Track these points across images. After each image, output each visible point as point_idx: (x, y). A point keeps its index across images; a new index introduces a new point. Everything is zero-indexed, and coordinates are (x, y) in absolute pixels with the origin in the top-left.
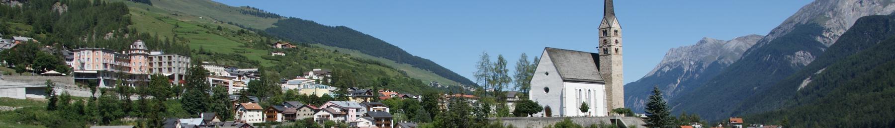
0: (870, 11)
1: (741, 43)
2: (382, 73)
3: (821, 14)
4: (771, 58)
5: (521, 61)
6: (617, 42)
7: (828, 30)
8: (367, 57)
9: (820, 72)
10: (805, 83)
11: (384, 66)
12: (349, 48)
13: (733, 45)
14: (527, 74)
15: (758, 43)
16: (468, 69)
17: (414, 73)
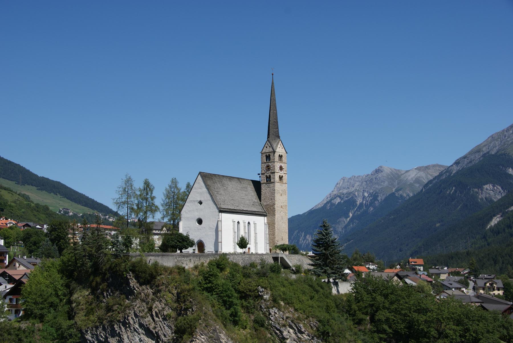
1: (422, 174)
4: (455, 191)
5: (170, 187)
6: (281, 168)
10: (495, 221)
13: (412, 176)
14: (177, 202)
15: (441, 174)
16: (107, 195)
17: (38, 197)
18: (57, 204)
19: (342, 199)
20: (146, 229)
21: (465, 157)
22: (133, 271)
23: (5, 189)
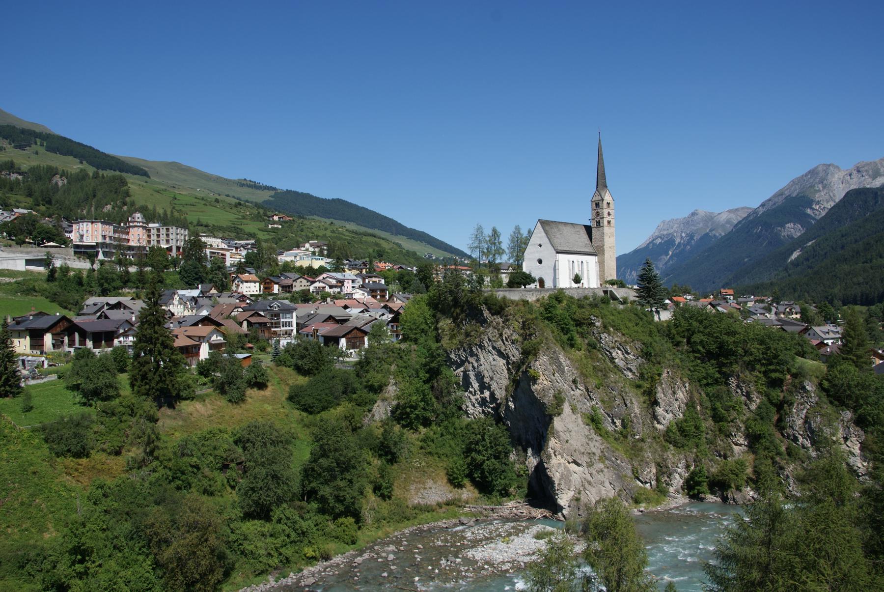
0: (860, 183)
1: (732, 216)
2: (377, 244)
3: (811, 187)
4: (762, 230)
7: (818, 203)
8: (362, 229)
9: (810, 243)
10: (795, 255)
11: (380, 238)
12: (345, 220)
13: (724, 217)
14: (520, 245)
15: (749, 216)
16: (462, 241)
17: (408, 245)
18: (423, 250)
19: (663, 239)
20: (495, 269)
21: (770, 200)
22: (486, 304)
23: (383, 239)
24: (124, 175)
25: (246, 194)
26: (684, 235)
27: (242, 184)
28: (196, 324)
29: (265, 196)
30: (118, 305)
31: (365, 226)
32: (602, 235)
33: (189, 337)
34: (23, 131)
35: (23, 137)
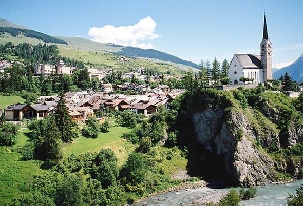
24: (57, 44)
25: (110, 49)
26: (212, 128)
27: (109, 45)
28: (82, 106)
29: (119, 49)
30: (51, 99)
31: (164, 60)
32: (271, 59)
33: (78, 111)
34: (15, 29)
35: (14, 32)
